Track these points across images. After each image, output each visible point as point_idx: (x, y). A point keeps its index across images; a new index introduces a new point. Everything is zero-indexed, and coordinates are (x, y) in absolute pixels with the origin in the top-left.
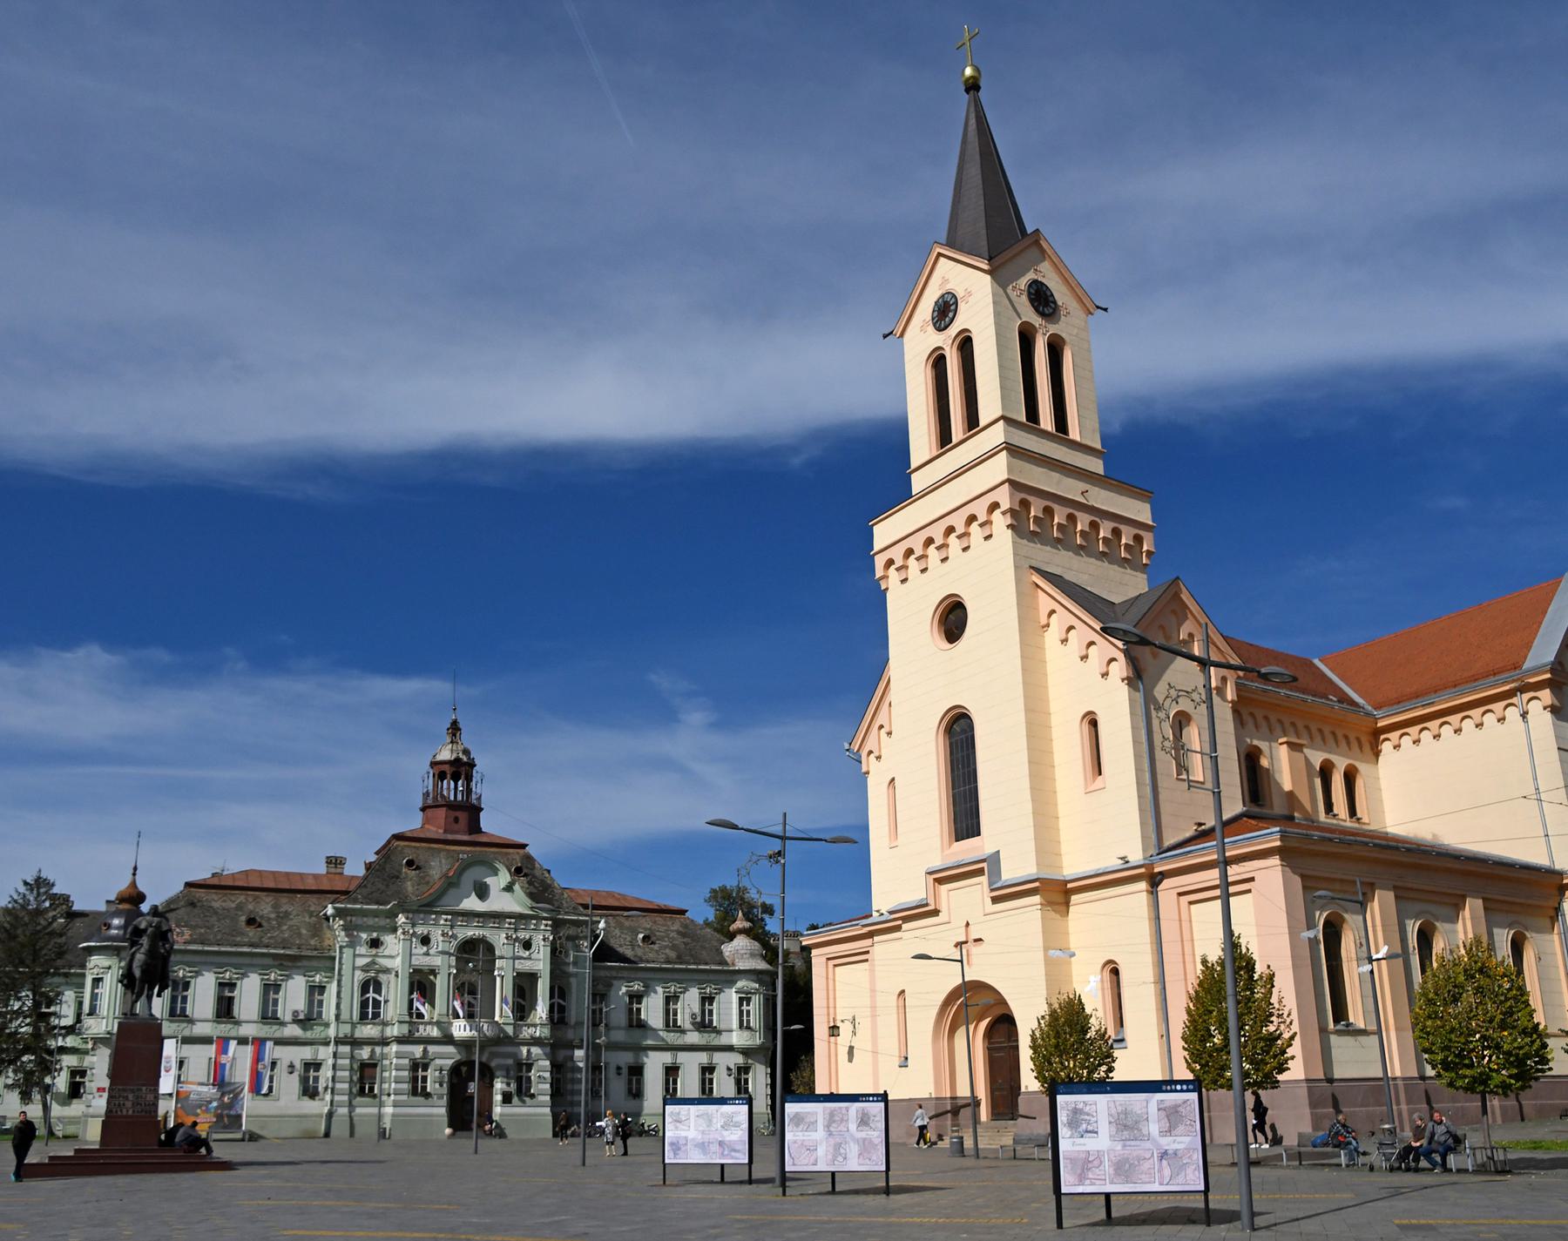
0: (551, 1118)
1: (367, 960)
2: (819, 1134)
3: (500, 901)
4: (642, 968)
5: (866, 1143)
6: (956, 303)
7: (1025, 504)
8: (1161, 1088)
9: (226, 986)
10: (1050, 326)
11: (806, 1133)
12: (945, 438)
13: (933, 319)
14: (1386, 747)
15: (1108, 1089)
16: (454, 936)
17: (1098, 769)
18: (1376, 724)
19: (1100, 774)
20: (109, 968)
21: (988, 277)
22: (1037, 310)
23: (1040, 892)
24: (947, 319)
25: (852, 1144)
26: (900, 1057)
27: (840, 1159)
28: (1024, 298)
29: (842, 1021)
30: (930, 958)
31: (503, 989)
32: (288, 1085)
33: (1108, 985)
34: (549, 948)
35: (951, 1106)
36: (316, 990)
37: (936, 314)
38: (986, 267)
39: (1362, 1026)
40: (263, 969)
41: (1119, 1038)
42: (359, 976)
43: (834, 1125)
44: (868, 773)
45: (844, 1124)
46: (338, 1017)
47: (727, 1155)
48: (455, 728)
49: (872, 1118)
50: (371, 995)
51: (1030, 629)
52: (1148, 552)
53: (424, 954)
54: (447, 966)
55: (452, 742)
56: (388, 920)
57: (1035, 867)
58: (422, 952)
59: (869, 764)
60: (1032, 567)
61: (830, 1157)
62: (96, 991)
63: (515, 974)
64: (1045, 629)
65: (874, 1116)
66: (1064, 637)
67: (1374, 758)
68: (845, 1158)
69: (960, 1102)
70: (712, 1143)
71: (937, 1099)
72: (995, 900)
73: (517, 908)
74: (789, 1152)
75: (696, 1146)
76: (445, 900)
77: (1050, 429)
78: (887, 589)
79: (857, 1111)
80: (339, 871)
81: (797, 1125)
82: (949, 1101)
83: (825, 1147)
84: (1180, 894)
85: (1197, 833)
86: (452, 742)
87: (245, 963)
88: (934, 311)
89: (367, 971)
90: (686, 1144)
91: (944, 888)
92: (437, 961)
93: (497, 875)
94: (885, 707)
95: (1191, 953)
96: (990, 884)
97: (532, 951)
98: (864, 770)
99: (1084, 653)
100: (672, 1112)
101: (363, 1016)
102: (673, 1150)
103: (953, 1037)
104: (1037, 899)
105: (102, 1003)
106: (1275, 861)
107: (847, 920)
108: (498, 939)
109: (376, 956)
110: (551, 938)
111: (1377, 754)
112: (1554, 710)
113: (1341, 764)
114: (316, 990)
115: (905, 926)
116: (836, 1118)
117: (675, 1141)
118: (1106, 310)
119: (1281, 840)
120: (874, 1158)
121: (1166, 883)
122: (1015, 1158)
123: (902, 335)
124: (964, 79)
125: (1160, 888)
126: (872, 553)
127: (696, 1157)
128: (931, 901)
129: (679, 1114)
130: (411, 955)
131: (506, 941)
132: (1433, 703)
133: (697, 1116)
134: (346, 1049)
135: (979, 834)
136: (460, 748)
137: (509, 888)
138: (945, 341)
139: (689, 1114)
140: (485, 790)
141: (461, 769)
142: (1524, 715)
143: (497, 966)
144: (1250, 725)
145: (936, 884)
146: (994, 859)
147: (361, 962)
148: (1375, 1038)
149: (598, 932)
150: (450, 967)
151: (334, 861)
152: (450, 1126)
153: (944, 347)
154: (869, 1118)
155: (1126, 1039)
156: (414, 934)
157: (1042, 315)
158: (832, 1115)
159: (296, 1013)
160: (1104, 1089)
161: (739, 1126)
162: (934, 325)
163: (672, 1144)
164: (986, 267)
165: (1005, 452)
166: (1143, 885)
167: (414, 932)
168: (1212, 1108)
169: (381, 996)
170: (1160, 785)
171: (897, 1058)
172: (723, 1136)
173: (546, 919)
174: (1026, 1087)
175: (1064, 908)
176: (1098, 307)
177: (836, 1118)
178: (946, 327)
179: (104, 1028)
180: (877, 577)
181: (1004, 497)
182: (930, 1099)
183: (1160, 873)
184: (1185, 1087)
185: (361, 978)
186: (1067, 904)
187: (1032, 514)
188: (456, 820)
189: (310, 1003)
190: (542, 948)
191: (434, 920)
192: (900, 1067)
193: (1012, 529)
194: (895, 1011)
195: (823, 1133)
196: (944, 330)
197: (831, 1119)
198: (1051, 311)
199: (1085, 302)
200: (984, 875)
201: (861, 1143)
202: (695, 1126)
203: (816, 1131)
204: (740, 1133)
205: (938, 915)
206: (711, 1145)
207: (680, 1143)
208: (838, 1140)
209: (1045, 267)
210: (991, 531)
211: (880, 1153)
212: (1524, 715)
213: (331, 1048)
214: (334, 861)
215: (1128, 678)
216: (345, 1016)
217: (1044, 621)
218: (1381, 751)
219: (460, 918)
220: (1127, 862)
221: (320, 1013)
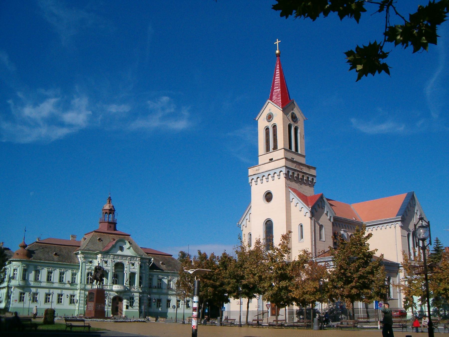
0: (139, 313)
4: (155, 271)
6: (273, 116)
7: (288, 172)
9: (50, 273)
10: (295, 124)
12: (268, 149)
16: (114, 261)
17: (302, 237)
19: (302, 238)
20: (19, 266)
24: (270, 120)
31: (126, 277)
32: (66, 300)
34: (139, 266)
36: (74, 275)
40: (60, 268)
42: (87, 271)
46: (81, 283)
48: (110, 199)
51: (288, 202)
53: (106, 266)
55: (109, 203)
56: (95, 256)
58: (105, 265)
62: (14, 272)
73: (130, 254)
76: (112, 251)
78: (251, 186)
80: (75, 239)
86: (109, 203)
87: (55, 266)
88: (267, 116)
89: (89, 270)
92: (109, 268)
93: (126, 244)
97: (134, 266)
98: (242, 229)
99: (300, 210)
105: (17, 276)
108: (126, 263)
109: (91, 266)
110: (140, 263)
112: (401, 227)
114: (74, 275)
130: (130, 268)
131: (128, 263)
134: (83, 291)
136: (112, 205)
137: (129, 248)
138: (270, 125)
140: (119, 218)
142: (395, 227)
143: (125, 270)
144: (335, 226)
147: (87, 267)
149: (151, 261)
150: (113, 270)
152: (112, 314)
157: (294, 121)
159: (69, 281)
162: (267, 120)
167: (104, 260)
170: (316, 242)
173: (139, 257)
179: (17, 283)
181: (284, 170)
187: (290, 174)
188: (110, 227)
189: (72, 278)
190: (137, 266)
191: (109, 257)
196: (270, 122)
213: (78, 291)
215: (310, 217)
216: (83, 282)
219: (116, 256)
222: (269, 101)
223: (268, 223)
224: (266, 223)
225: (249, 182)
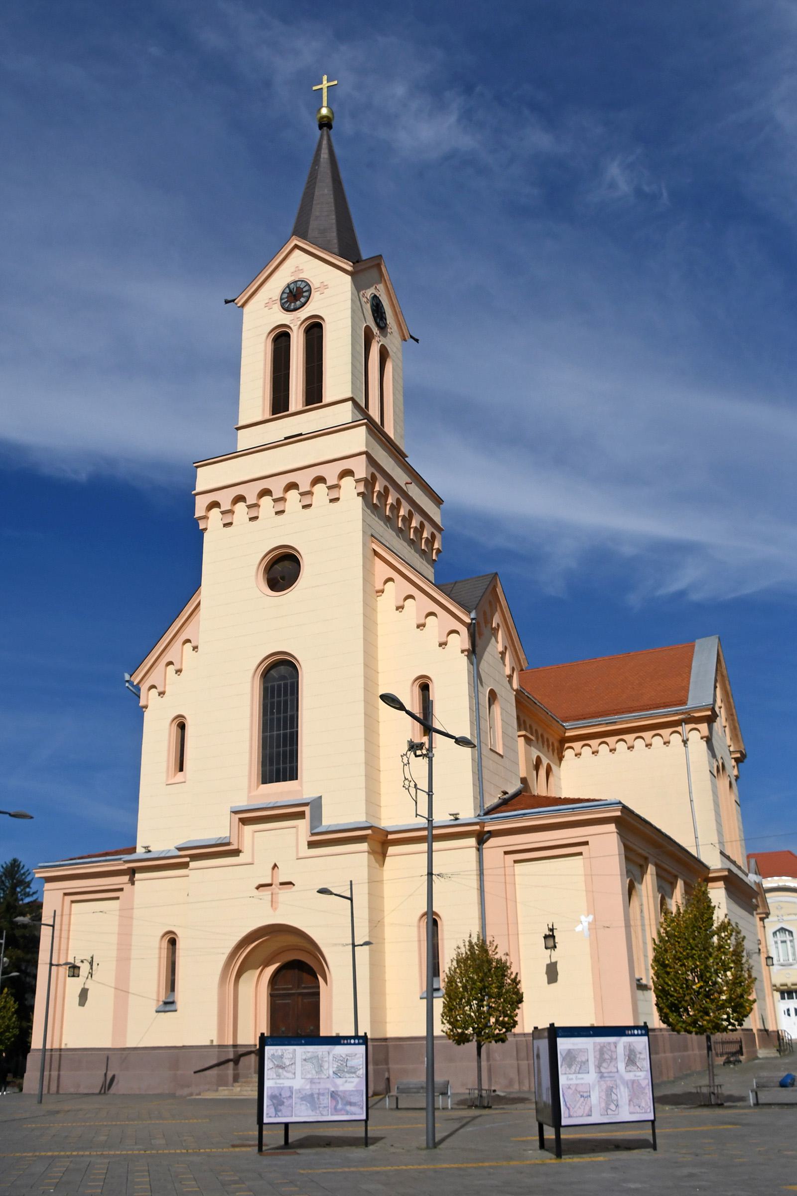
2: (591, 1077)
5: (635, 1085)
6: (310, 291)
7: (374, 478)
8: (625, 1032)
10: (382, 338)
11: (580, 1076)
13: (281, 299)
14: (568, 754)
15: (591, 1033)
18: (565, 733)
19: (181, 769)
21: (349, 277)
23: (368, 840)
24: (298, 303)
25: (622, 1088)
26: (158, 1001)
27: (613, 1107)
28: (369, 305)
29: (82, 962)
30: (331, 893)
33: (164, 953)
35: (234, 1054)
37: (285, 295)
38: (349, 268)
41: (170, 1000)
43: (605, 1065)
44: (146, 707)
45: (613, 1063)
47: (341, 1110)
49: (638, 1056)
52: (438, 550)
57: (364, 815)
59: (149, 698)
61: (603, 1105)
64: (378, 594)
65: (640, 1053)
66: (400, 603)
67: (558, 761)
68: (617, 1106)
69: (241, 1051)
70: (323, 1094)
71: (219, 1046)
72: (312, 845)
74: (565, 1101)
75: (303, 1099)
78: (206, 529)
79: (625, 1047)
81: (570, 1066)
82: (232, 1049)
83: (597, 1093)
84: (65, 894)
85: (500, 801)
88: (283, 293)
90: (291, 1097)
91: (248, 829)
95: (66, 937)
96: (312, 828)
100: (273, 1055)
102: (274, 1104)
103: (239, 980)
104: (364, 846)
106: (612, 827)
107: (85, 854)
111: (561, 758)
113: (545, 761)
115: (192, 865)
116: (607, 1056)
117: (277, 1093)
118: (417, 341)
119: (621, 812)
120: (643, 1104)
121: (493, 842)
122: (397, 1108)
123: (243, 306)
124: (319, 116)
125: (485, 845)
126: (193, 492)
127: (301, 1114)
128: (234, 840)
129: (281, 1057)
132: (615, 722)
133: (305, 1060)
135: (297, 779)
138: (295, 322)
139: (294, 1057)
142: (685, 742)
145: (240, 823)
146: (316, 804)
153: (291, 326)
154: (635, 1056)
155: (176, 1000)
158: (602, 1051)
160: (299, 1042)
161: (355, 1073)
162: (282, 306)
163: (273, 1097)
165: (364, 427)
166: (472, 841)
168: (62, 1067)
171: (155, 1002)
172: (335, 1085)
174: (66, 1044)
175: (381, 858)
176: (411, 337)
177: (607, 1056)
178: (295, 310)
180: (197, 515)
181: (361, 468)
182: (211, 1046)
183: (489, 832)
184: (357, 1041)
186: (384, 855)
192: (157, 1012)
193: (363, 498)
194: (157, 951)
195: (596, 1075)
197: (603, 1058)
199: (403, 328)
200: (304, 818)
201: (630, 1085)
202: (302, 1074)
203: (588, 1073)
204: (356, 1080)
205: (238, 856)
206: (321, 1097)
207: (284, 1096)
208: (610, 1083)
209: (381, 287)
210: (207, 525)
211: (647, 1098)
212: (685, 742)
215: (468, 650)
217: (379, 586)
218: (564, 757)
220: (457, 819)
222: (295, 241)
223: (272, 672)
224: (266, 675)
225: (197, 515)
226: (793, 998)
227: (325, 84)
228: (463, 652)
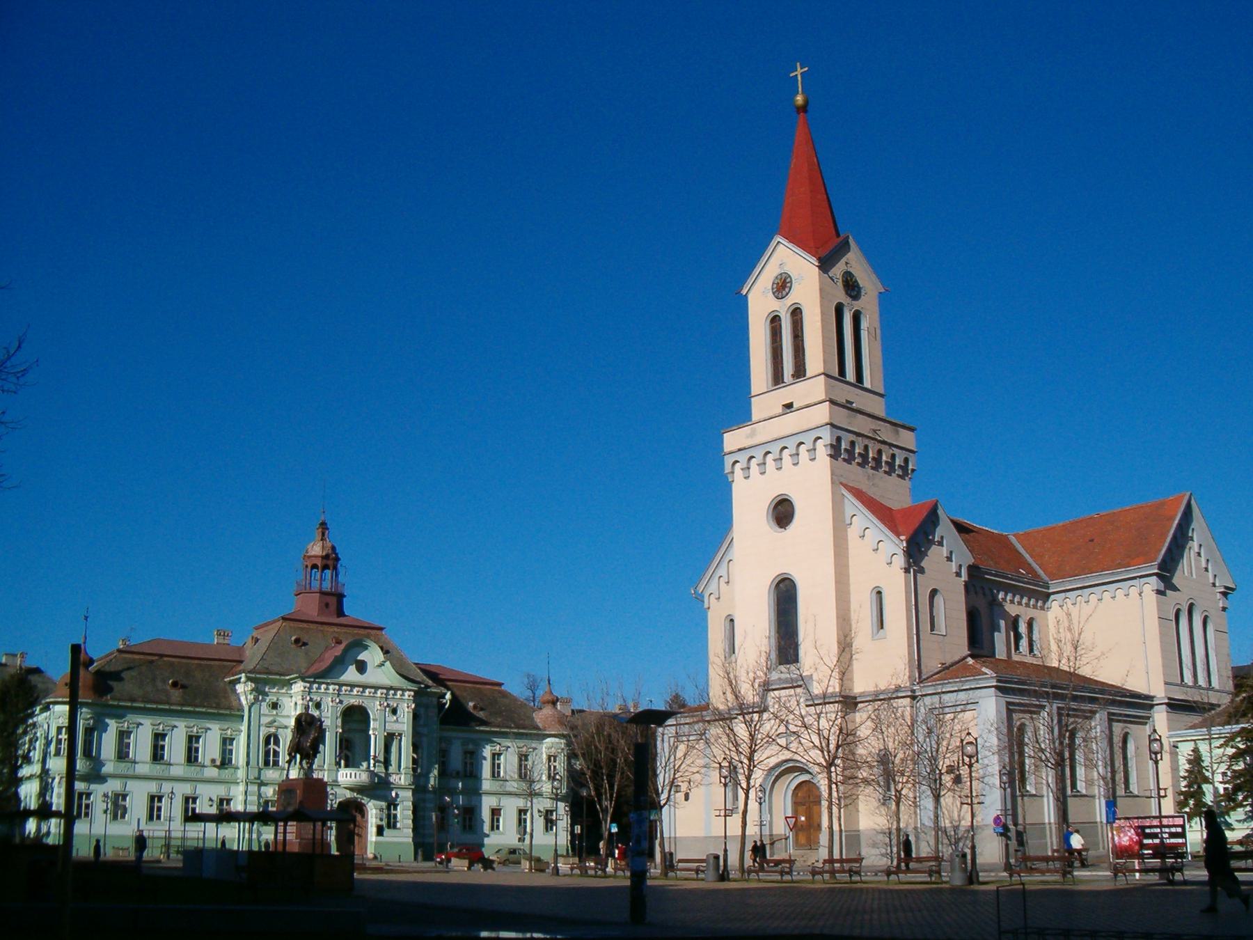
1: (270, 719)
3: (372, 676)
7: (839, 439)
12: (778, 378)
13: (773, 289)
19: (882, 628)
22: (847, 293)
39: (1034, 792)
42: (264, 732)
50: (272, 746)
51: (840, 527)
53: (395, 722)
54: (335, 727)
55: (322, 540)
60: (841, 483)
63: (386, 734)
77: (852, 381)
86: (322, 540)
94: (724, 564)
101: (267, 763)
136: (329, 545)
140: (351, 580)
141: (330, 561)
147: (265, 720)
148: (727, 808)
151: (222, 634)
156: (388, 705)
159: (213, 761)
164: (817, 264)
169: (279, 747)
173: (410, 690)
180: (726, 472)
181: (827, 436)
185: (265, 733)
188: (327, 605)
190: (330, 708)
198: (855, 293)
214: (222, 634)
221: (230, 760)
223: (781, 585)
225: (726, 472)
226: (1169, 731)
227: (799, 71)
228: (901, 569)
